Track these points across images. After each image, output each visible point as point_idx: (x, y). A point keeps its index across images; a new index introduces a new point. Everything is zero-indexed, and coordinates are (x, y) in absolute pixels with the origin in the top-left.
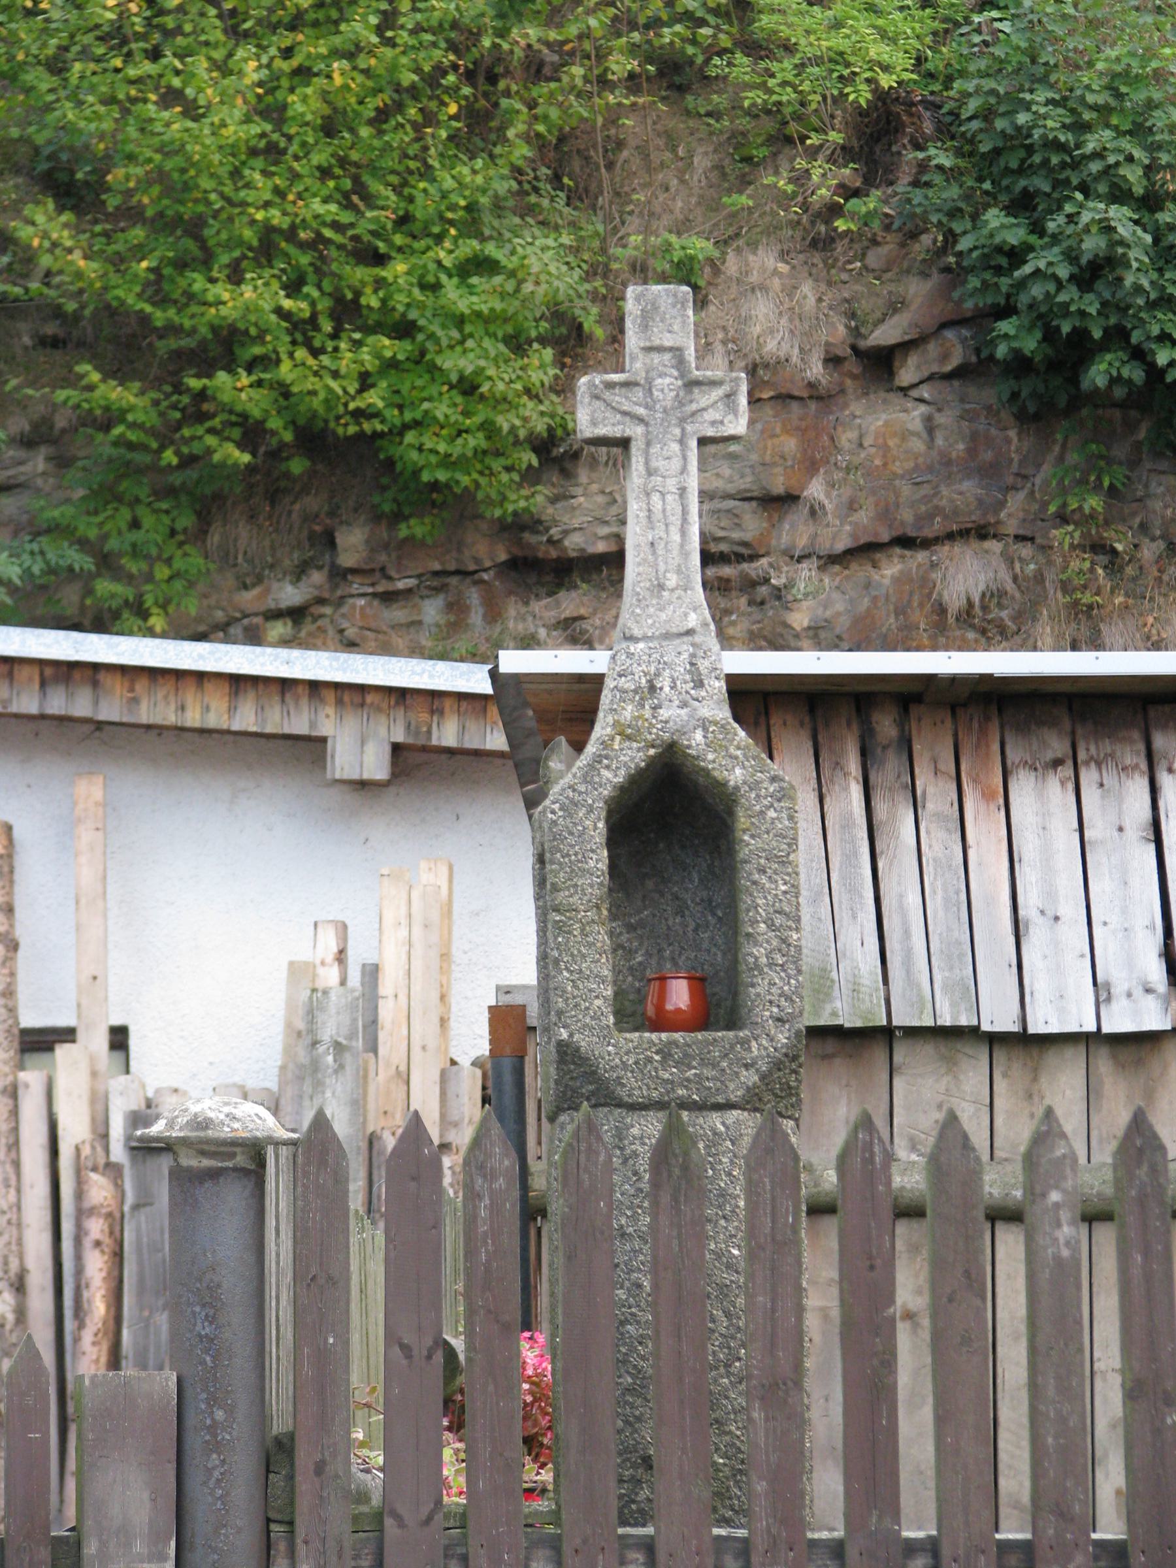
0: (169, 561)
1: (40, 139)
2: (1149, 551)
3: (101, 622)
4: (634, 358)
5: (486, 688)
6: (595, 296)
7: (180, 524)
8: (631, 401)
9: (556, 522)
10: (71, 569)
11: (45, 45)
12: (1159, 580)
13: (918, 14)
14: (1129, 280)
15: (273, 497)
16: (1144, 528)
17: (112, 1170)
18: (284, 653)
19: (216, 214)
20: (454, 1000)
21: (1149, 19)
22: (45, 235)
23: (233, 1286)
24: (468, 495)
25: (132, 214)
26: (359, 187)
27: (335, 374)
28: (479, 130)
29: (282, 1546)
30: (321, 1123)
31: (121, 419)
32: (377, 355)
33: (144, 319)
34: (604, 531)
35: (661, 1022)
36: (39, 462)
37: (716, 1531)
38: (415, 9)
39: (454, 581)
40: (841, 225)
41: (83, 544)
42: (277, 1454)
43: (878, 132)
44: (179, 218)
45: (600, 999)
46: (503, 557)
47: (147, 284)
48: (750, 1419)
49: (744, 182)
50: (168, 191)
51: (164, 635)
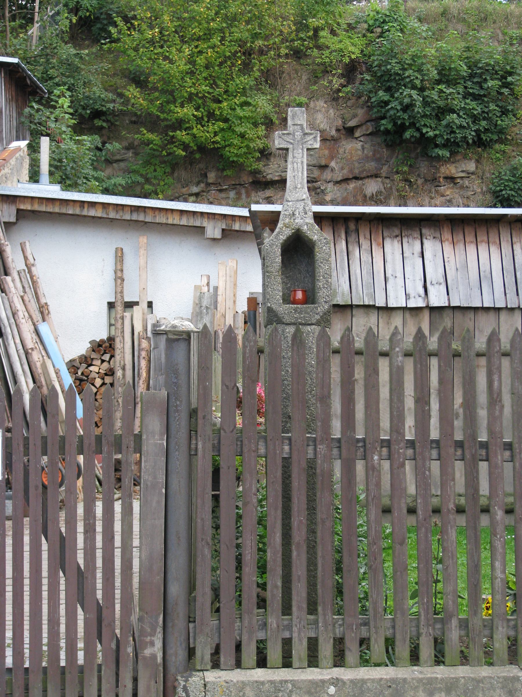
0: (164, 180)
1: (131, 69)
2: (420, 181)
3: (146, 196)
4: (290, 127)
5: (248, 214)
6: (276, 112)
7: (167, 171)
8: (289, 139)
9: (265, 172)
10: (138, 182)
11: (133, 44)
12: (422, 189)
13: (362, 39)
14: (416, 110)
15: (191, 164)
16: (419, 175)
17: (148, 339)
18: (194, 204)
19: (177, 89)
20: (237, 296)
21: (423, 41)
22: (133, 94)
23: (182, 368)
24: (242, 165)
25: (155, 89)
26: (215, 83)
27: (208, 132)
28: (246, 68)
29: (194, 437)
30: (205, 326)
31: (152, 143)
32: (219, 127)
33: (158, 117)
34: (278, 174)
35: (294, 302)
36: (130, 154)
37: (307, 435)
38: (230, 36)
39: (238, 186)
40: (341, 94)
41: (142, 175)
42: (193, 413)
43: (351, 70)
44: (167, 90)
45: (279, 295)
46: (251, 181)
47: (159, 108)
48: (317, 406)
49: (315, 83)
50: (165, 83)
51: (162, 199)
